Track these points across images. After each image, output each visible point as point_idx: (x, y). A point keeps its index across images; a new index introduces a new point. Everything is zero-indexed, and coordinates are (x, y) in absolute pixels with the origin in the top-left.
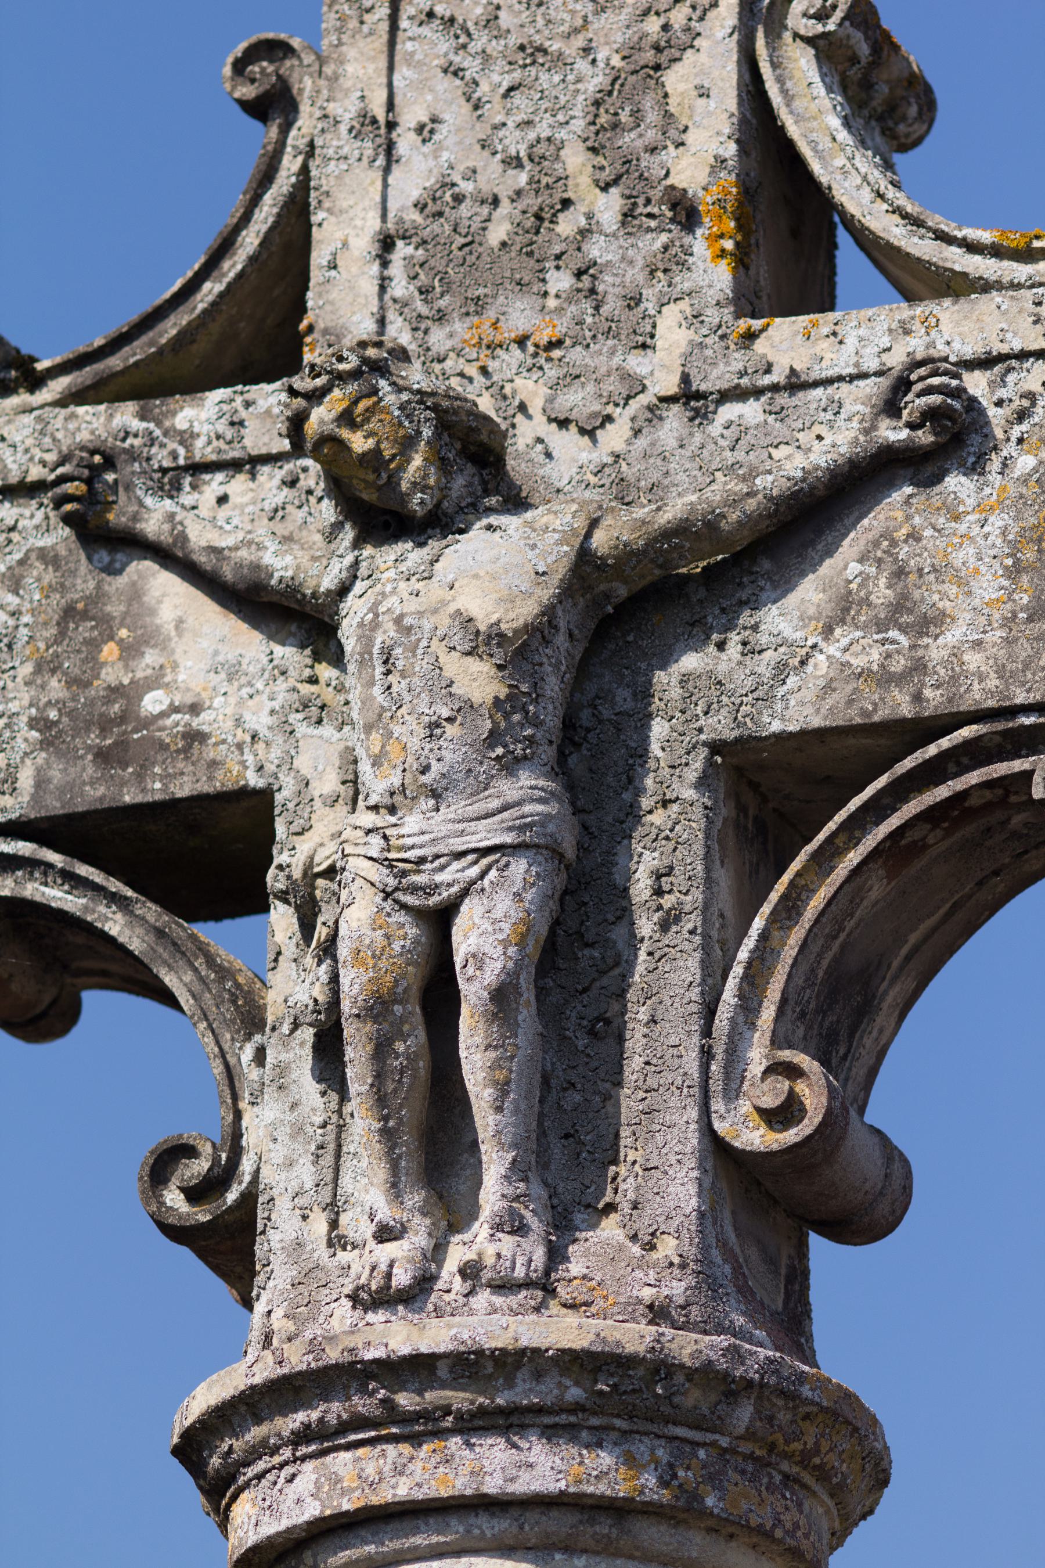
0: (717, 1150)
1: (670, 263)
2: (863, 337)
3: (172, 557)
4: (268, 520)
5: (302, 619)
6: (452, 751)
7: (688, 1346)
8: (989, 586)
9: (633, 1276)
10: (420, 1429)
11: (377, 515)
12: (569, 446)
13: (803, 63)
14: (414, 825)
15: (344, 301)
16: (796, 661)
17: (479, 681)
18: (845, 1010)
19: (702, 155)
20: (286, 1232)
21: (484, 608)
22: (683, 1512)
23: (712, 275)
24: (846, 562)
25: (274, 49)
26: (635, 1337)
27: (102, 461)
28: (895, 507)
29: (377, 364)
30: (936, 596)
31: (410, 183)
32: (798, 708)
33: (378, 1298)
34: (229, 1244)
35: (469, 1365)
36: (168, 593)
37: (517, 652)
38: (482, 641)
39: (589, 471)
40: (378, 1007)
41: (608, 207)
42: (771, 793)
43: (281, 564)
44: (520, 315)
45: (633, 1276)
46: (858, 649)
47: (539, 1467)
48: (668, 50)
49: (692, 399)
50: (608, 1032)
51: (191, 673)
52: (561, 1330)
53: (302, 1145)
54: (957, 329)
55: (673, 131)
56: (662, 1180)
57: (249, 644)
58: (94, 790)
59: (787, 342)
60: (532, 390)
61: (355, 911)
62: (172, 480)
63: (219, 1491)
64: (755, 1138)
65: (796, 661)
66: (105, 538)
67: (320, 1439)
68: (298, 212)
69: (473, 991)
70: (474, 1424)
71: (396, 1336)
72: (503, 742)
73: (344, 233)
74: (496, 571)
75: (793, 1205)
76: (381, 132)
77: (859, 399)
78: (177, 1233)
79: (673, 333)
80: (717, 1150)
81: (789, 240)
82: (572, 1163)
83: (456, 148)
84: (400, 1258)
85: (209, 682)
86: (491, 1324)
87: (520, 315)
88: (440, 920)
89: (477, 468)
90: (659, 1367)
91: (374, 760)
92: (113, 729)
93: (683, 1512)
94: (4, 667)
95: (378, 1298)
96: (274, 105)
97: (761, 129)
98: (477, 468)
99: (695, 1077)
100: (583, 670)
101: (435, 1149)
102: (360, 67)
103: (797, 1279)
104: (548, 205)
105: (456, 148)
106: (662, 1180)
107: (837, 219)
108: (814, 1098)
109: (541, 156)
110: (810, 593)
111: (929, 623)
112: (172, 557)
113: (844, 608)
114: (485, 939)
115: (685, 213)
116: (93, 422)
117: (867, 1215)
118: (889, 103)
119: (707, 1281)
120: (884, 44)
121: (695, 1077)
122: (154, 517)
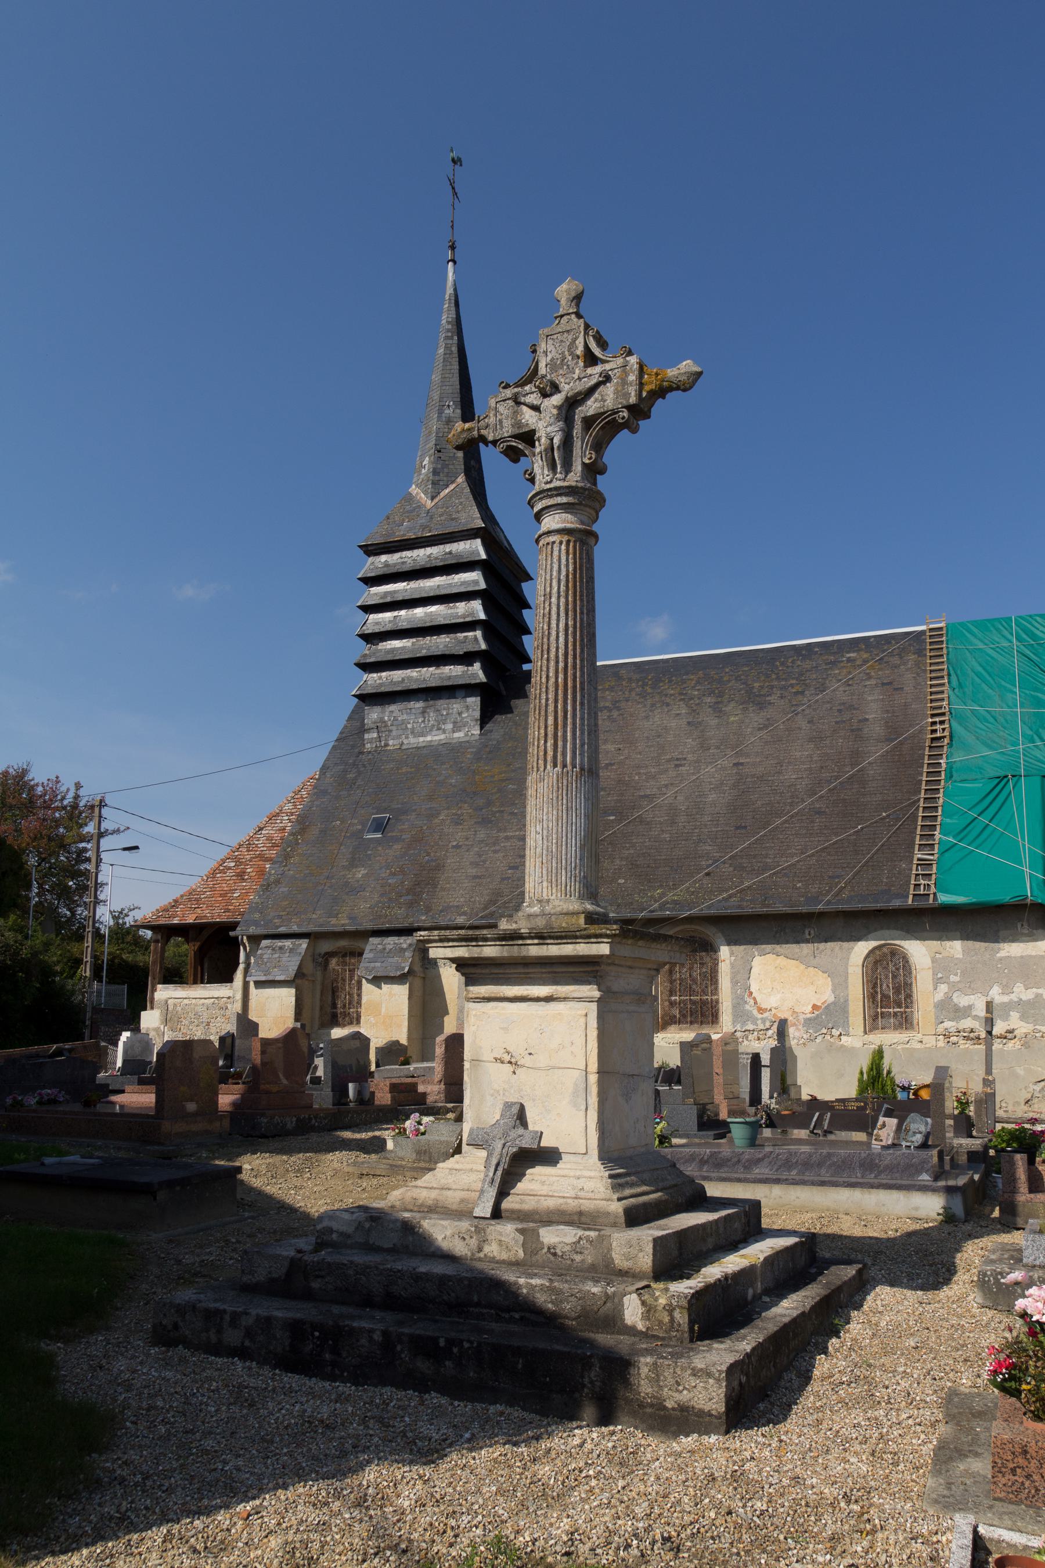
0: (583, 463)
1: (577, 363)
2: (598, 369)
3: (525, 404)
4: (534, 399)
5: (536, 408)
6: (552, 420)
7: (580, 485)
8: (612, 396)
9: (575, 478)
10: (551, 496)
11: (545, 395)
12: (567, 386)
13: (591, 338)
14: (549, 429)
15: (542, 370)
16: (591, 407)
17: (555, 412)
18: (599, 447)
19: (580, 350)
20: (538, 478)
21: (555, 403)
22: (580, 504)
23: (581, 364)
24: (596, 395)
25: (534, 345)
26: (574, 484)
27: (518, 393)
28: (602, 388)
29: (543, 377)
30: (606, 398)
31: (549, 358)
32: (591, 412)
33: (547, 483)
34: (532, 480)
35: (556, 488)
36: (525, 408)
37: (559, 408)
38: (555, 407)
39: (567, 388)
40: (545, 450)
41: (570, 358)
42: (588, 422)
43: (535, 403)
44: (561, 372)
45: (575, 478)
46: (597, 405)
47: (564, 500)
48: (576, 339)
49: (580, 379)
50: (571, 451)
51: (527, 417)
52: (566, 484)
53: (540, 468)
54: (607, 366)
55: (577, 348)
56: (577, 467)
57: (533, 413)
58: (517, 431)
59: (589, 371)
60: (562, 380)
61: (543, 440)
62: (524, 396)
63: (532, 507)
64: (587, 461)
65: (591, 407)
66: (518, 403)
67: (541, 499)
68: (537, 363)
69: (555, 447)
70: (557, 495)
71: (548, 486)
72: (558, 418)
73: (542, 365)
74: (557, 399)
75: (593, 470)
76: (546, 353)
77: (597, 376)
78: (528, 480)
79: (577, 371)
80: (583, 463)
81: (591, 359)
82: (568, 467)
83: (554, 353)
84: (548, 478)
85: (528, 417)
86: (558, 484)
87: (561, 372)
88: (552, 440)
89: (555, 388)
90: (577, 487)
91: (545, 425)
92: (518, 424)
93: (580, 504)
94: (1041, 1273)
95: (547, 483)
96: (534, 351)
97: (587, 347)
98: (555, 388)
99: (582, 455)
100: (568, 411)
101: (553, 467)
102: (543, 345)
103: (595, 479)
104: (564, 358)
105: (554, 353)
106: (577, 467)
107: (644, 394)
108: (593, 456)
109: (563, 353)
110: (592, 399)
111: (605, 401)
112: (525, 404)
113: (596, 400)
114: (556, 441)
115: (578, 357)
116: (516, 390)
117: (602, 472)
118: (603, 344)
119: (583, 478)
120: (601, 336)
121: (582, 455)
122: (522, 399)
